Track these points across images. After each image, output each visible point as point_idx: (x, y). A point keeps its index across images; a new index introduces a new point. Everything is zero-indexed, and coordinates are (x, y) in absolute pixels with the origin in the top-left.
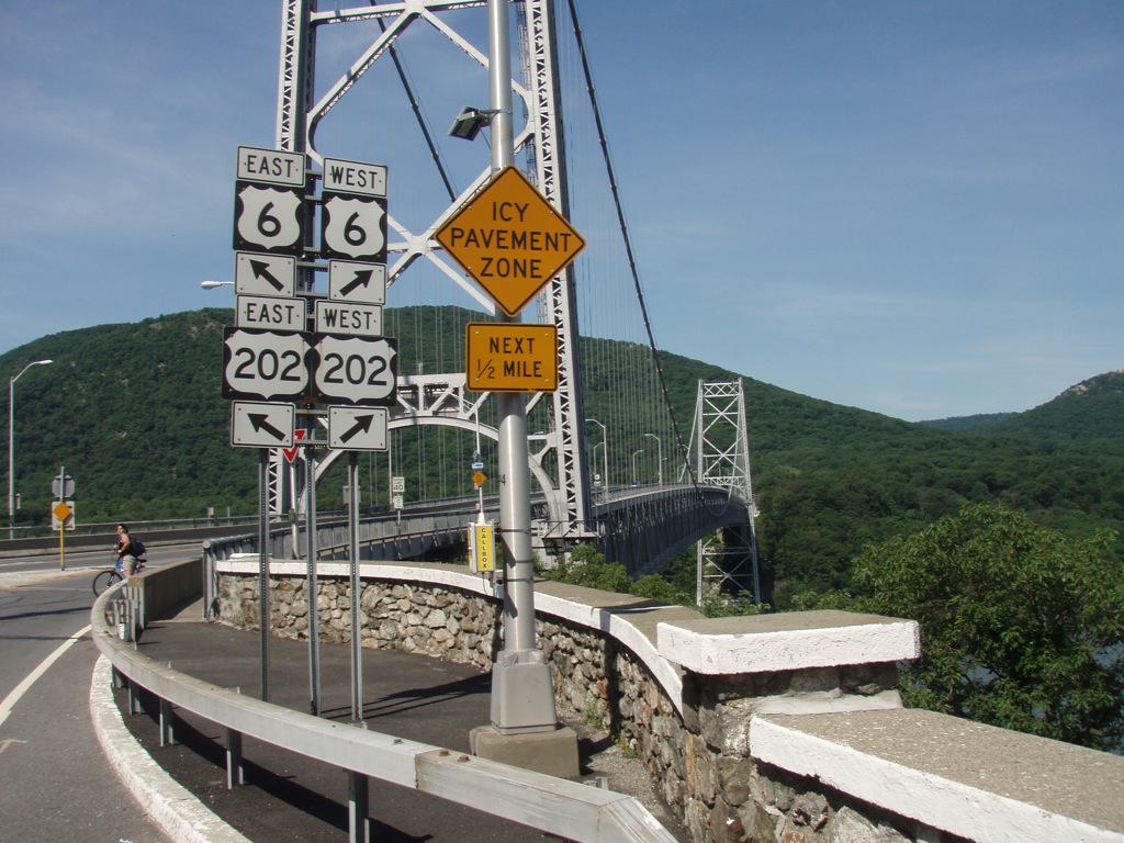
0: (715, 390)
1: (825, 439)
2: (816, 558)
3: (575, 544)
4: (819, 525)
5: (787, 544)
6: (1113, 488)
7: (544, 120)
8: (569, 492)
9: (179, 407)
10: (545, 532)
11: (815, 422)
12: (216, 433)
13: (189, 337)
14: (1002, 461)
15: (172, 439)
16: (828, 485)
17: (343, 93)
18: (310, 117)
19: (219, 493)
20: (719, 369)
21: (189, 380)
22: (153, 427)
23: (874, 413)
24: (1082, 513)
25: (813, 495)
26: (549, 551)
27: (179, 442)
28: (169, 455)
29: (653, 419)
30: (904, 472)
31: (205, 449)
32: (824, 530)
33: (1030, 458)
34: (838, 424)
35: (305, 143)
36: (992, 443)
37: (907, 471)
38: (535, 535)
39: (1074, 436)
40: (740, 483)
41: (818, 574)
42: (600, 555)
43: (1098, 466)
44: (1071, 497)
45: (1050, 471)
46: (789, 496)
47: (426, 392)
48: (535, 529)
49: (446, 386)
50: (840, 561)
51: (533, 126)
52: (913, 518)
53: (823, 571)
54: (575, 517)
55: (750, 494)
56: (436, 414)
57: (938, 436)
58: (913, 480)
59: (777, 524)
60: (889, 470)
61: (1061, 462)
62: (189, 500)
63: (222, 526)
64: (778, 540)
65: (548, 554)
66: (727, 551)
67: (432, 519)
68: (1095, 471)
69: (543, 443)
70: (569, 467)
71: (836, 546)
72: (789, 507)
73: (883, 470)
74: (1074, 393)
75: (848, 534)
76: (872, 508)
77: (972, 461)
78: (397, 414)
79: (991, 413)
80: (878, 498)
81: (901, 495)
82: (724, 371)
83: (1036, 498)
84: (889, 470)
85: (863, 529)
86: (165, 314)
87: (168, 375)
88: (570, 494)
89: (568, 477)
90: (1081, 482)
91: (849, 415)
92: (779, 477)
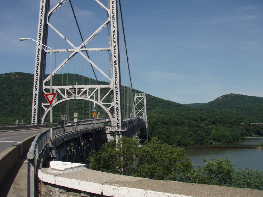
0: (139, 95)
1: (162, 108)
2: (161, 136)
3: (118, 133)
4: (162, 128)
6: (229, 121)
7: (113, 17)
9: (9, 95)
10: (111, 129)
12: (18, 102)
13: (11, 79)
14: (203, 114)
15: (7, 103)
17: (58, 8)
18: (49, 14)
19: (18, 117)
20: (138, 91)
21: (11, 89)
22: (2, 100)
23: (174, 102)
24: (223, 126)
25: (161, 121)
26: (111, 134)
27: (8, 104)
28: (6, 107)
29: (126, 101)
31: (14, 106)
32: (163, 129)
33: (210, 113)
34: (165, 104)
35: (47, 21)
36: (201, 110)
37: (182, 116)
38: (108, 130)
40: (144, 117)
41: (162, 139)
43: (225, 115)
44: (220, 123)
46: (155, 121)
47: (78, 90)
48: (108, 128)
49: (84, 89)
50: (167, 137)
51: (110, 19)
52: (184, 127)
53: (163, 139)
55: (146, 120)
56: (81, 96)
57: (188, 108)
59: (152, 128)
61: (217, 114)
62: (10, 118)
63: (20, 126)
65: (111, 135)
66: (141, 133)
67: (83, 125)
69: (110, 105)
70: (118, 112)
71: (166, 133)
72: (155, 123)
74: (219, 98)
77: (197, 114)
78: (70, 96)
79: (200, 103)
80: (176, 122)
82: (139, 91)
83: (212, 123)
84: (178, 115)
85: (173, 129)
86: (6, 73)
87: (6, 88)
88: (118, 119)
89: (117, 114)
90: (222, 119)
91: (168, 102)
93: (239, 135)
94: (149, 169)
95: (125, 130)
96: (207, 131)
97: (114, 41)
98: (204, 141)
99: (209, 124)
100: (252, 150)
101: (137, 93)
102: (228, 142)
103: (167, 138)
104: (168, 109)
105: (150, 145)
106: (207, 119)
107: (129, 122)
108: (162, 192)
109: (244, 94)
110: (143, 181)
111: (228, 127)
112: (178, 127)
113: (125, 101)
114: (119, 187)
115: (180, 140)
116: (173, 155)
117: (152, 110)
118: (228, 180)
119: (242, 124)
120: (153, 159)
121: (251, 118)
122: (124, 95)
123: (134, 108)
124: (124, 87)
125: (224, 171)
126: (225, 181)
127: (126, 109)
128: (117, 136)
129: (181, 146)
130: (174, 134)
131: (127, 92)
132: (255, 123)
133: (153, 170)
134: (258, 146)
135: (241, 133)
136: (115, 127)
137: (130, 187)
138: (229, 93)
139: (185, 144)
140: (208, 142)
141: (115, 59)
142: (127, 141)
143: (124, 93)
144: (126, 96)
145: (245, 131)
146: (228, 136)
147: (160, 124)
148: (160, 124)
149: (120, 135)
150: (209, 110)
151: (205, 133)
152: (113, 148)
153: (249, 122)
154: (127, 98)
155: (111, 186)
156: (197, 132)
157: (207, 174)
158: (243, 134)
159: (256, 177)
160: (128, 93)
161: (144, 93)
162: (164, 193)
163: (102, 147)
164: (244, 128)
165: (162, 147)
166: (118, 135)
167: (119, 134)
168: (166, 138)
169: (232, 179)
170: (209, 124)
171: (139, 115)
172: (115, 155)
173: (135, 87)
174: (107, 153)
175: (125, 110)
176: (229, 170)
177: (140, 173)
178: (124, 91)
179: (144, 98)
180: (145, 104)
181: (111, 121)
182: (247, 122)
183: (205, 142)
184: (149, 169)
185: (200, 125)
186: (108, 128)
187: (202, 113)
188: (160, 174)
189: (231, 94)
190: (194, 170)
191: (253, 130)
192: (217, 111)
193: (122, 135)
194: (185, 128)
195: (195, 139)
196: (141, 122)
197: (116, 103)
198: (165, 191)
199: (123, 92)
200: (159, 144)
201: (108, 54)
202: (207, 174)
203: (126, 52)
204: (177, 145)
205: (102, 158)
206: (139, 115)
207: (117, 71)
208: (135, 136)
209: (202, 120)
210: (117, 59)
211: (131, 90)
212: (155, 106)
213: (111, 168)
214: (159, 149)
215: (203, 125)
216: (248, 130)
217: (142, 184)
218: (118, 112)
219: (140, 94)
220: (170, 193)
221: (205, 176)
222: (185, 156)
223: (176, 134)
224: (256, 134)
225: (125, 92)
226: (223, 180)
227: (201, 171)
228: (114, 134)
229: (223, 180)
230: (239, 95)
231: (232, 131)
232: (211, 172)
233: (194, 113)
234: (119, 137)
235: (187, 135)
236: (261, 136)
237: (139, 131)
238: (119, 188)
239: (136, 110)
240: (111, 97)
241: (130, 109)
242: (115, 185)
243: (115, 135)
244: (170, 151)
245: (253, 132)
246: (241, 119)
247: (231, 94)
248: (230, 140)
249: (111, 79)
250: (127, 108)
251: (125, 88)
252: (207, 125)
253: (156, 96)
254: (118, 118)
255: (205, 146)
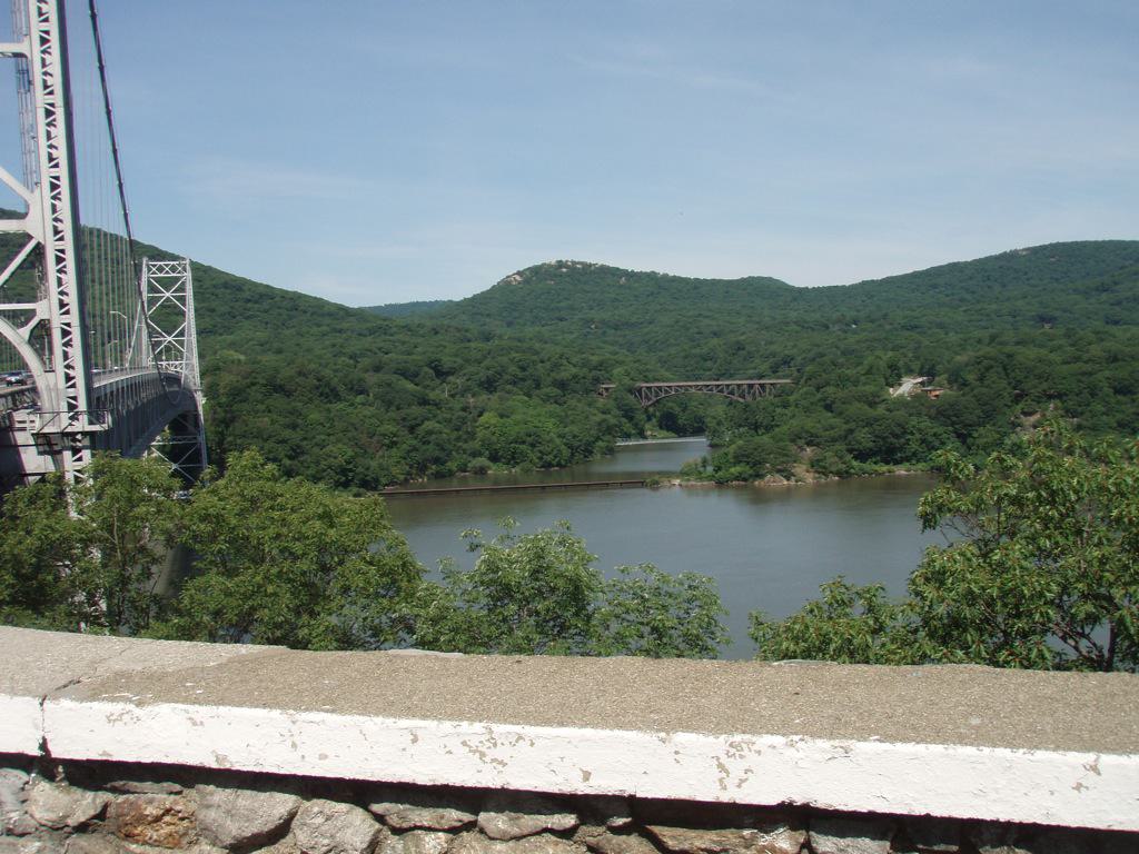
0: (161, 269)
1: (267, 323)
3: (75, 440)
4: (270, 411)
5: (237, 432)
8: (67, 375)
10: (37, 425)
11: (257, 306)
14: (445, 347)
16: (277, 370)
20: (157, 249)
23: (315, 298)
24: (526, 398)
26: (41, 448)
29: (105, 297)
30: (351, 358)
33: (473, 345)
34: (279, 308)
36: (434, 329)
38: (24, 429)
39: (509, 324)
40: (189, 369)
42: (270, 466)
43: (537, 353)
44: (514, 383)
45: (493, 358)
48: (24, 422)
50: (293, 450)
52: (363, 404)
54: (76, 407)
55: (198, 380)
58: (359, 366)
59: (226, 412)
60: (335, 356)
64: (227, 426)
65: (40, 453)
66: (174, 440)
68: (535, 358)
70: (67, 344)
71: (287, 433)
72: (237, 394)
73: (329, 355)
74: (510, 282)
75: (300, 421)
76: (321, 395)
77: (416, 347)
80: (328, 385)
81: (351, 382)
83: (481, 384)
84: (335, 356)
85: (314, 416)
88: (68, 378)
89: (66, 356)
90: (523, 369)
91: (292, 299)
92: (224, 363)
93: (592, 432)
94: (231, 595)
95: (105, 426)
96: (464, 421)
97: (41, 14)
98: (449, 464)
99: (466, 390)
100: (646, 491)
101: (152, 258)
102: (550, 465)
103: (291, 458)
104: (293, 329)
105: (226, 488)
106: (461, 367)
107: (123, 388)
108: (377, 715)
109: (611, 264)
110: (256, 659)
111: (547, 399)
112: (340, 406)
113: (98, 296)
114: (139, 704)
115: (348, 463)
116: (332, 526)
117: (221, 335)
118: (573, 621)
119: (607, 389)
120: (244, 551)
121: (639, 361)
122: (92, 269)
123: (140, 329)
124: (91, 231)
125: (561, 583)
126: (563, 628)
127: (106, 331)
128: (67, 455)
129: (355, 490)
130: (323, 437)
131: (106, 254)
132: (658, 380)
133: (246, 597)
134: (669, 475)
135: (600, 424)
136: (58, 413)
137: (196, 701)
138: (550, 258)
139: (368, 478)
140: (466, 465)
141: (50, 99)
142: (119, 472)
143: (96, 260)
144: (104, 273)
145: (615, 417)
146: (548, 438)
147: (260, 397)
148: (260, 397)
149: (85, 447)
150: (467, 331)
151: (452, 431)
152: (54, 508)
153: (632, 379)
154: (107, 282)
155: (95, 705)
156: (419, 425)
157: (484, 601)
158: (609, 430)
159: (689, 601)
160: (112, 259)
161: (184, 259)
162: (390, 721)
163: (5, 507)
164: (611, 402)
165: (282, 495)
166: (76, 451)
167: (78, 444)
168: (286, 456)
169: (589, 618)
170: (466, 390)
171: (164, 358)
172: (66, 540)
173: (143, 236)
174: (29, 533)
175: (99, 336)
176: (579, 578)
177: (190, 615)
178: (92, 249)
179: (183, 283)
180: (190, 309)
181: (39, 388)
182: (627, 381)
183: (452, 465)
184: (231, 595)
185: (432, 395)
186: (26, 418)
187: (441, 345)
188: (279, 615)
189: (561, 261)
190: (427, 589)
191: (651, 409)
192: (500, 337)
193: (93, 447)
194: (368, 411)
195: (413, 454)
196: (176, 388)
197: (56, 303)
198: (389, 708)
199: (87, 255)
200: (269, 480)
201: (13, 76)
202: (484, 601)
203: (101, 68)
204: (338, 485)
205: (8, 557)
206: (164, 358)
207: (61, 154)
208: (149, 455)
209: (441, 373)
210: (58, 99)
211: (126, 248)
212: (234, 317)
213: (53, 605)
214: (268, 504)
215: (442, 397)
216: (629, 414)
217: (261, 681)
218: (71, 346)
219: (167, 265)
220: (424, 717)
221: (477, 611)
222: (385, 527)
223: (329, 435)
224: (661, 428)
225: (99, 257)
226: (552, 623)
227: (459, 592)
228: (56, 448)
229: (552, 623)
230: (590, 265)
231: (567, 416)
232: (504, 592)
233: (404, 343)
234: (80, 459)
235: (375, 438)
236: (680, 437)
237: (166, 428)
238: (137, 711)
239: (150, 336)
240: (32, 279)
241: (121, 332)
242: (113, 700)
243: (60, 452)
244: (320, 511)
245: (649, 419)
246: (600, 366)
247: (560, 264)
248: (556, 457)
249: (32, 192)
250: (109, 327)
251: (99, 236)
252: (463, 396)
253: (239, 274)
254: (71, 372)
255: (454, 485)
